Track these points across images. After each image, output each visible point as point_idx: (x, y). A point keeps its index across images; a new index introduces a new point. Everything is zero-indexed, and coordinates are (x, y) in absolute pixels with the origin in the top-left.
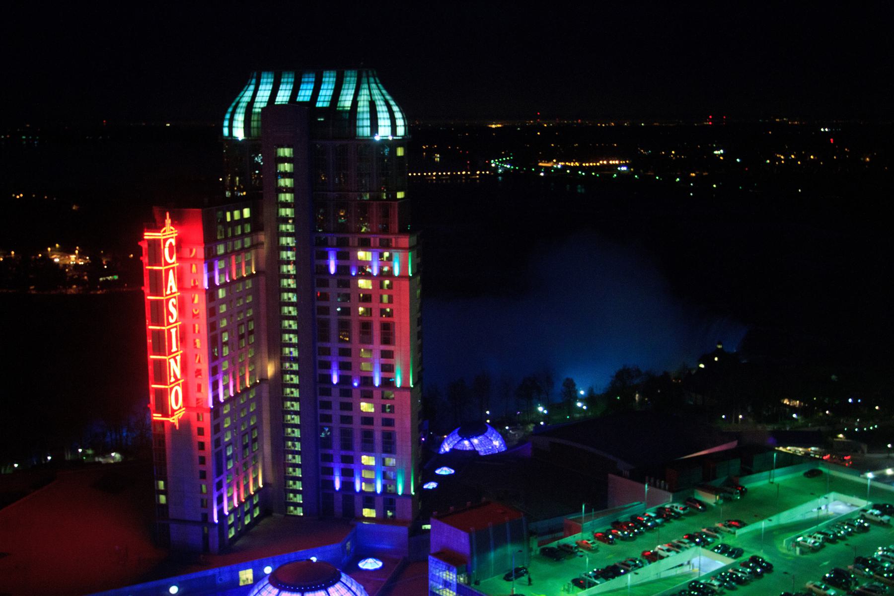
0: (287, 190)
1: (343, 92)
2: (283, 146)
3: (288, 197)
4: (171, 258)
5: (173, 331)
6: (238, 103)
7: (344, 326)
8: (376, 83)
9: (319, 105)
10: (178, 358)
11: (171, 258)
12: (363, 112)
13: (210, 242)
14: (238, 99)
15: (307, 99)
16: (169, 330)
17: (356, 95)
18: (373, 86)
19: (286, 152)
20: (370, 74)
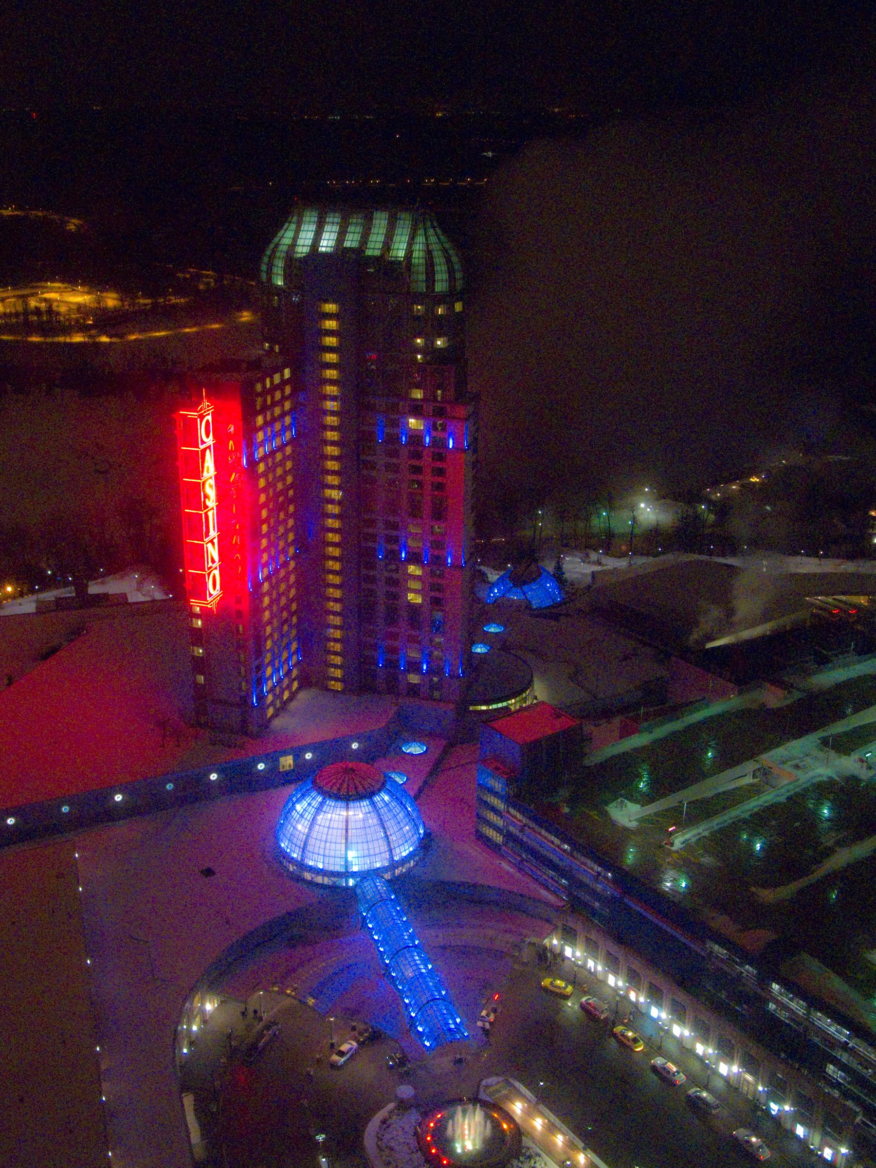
0: (332, 382)
1: (396, 238)
2: (326, 301)
3: (331, 537)
4: (208, 436)
5: (210, 514)
6: (277, 245)
7: (392, 616)
8: (434, 227)
9: (369, 253)
10: (216, 541)
11: (208, 436)
12: (418, 265)
13: (250, 412)
14: (276, 240)
15: (355, 245)
16: (206, 514)
17: (410, 244)
18: (431, 232)
19: (331, 307)
20: (429, 224)
